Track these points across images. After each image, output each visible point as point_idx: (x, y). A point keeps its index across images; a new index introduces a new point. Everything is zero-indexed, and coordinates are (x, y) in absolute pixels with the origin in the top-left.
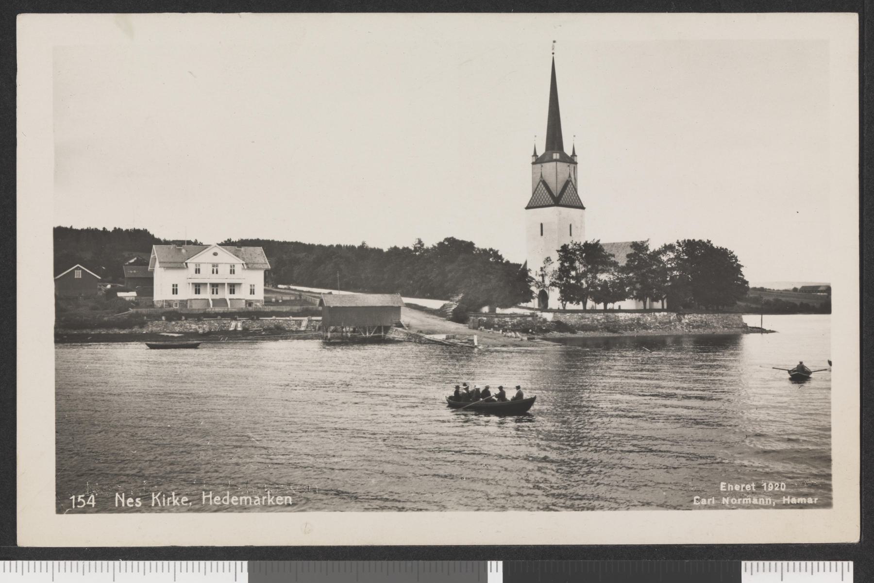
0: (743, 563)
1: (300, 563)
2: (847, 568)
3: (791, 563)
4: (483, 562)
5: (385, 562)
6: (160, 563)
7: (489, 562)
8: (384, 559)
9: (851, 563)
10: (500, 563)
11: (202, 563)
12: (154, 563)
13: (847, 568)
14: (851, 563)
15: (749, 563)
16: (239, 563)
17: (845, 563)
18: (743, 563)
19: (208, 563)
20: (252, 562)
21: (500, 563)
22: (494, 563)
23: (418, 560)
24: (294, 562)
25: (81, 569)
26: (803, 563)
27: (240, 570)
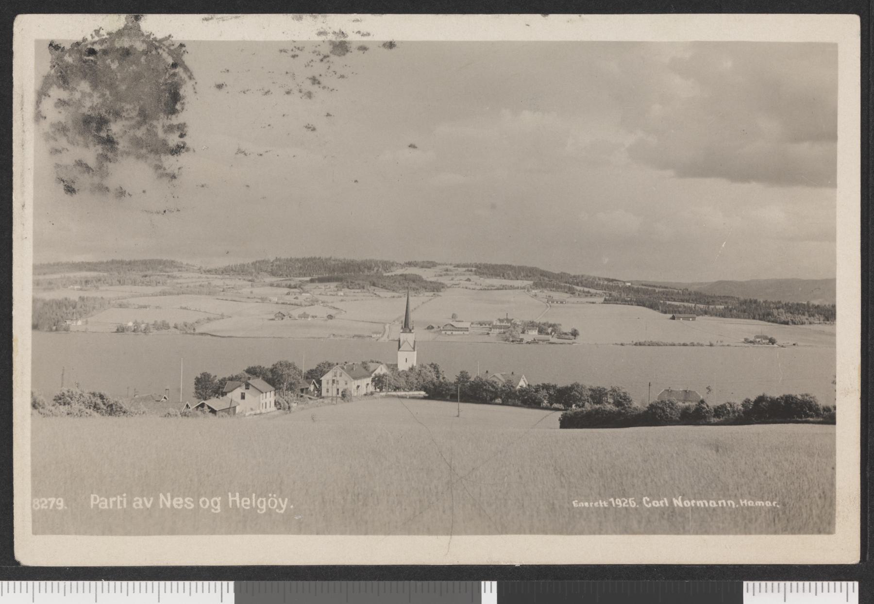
0: (745, 583)
1: (288, 583)
2: (852, 588)
3: (794, 583)
4: (475, 583)
5: (375, 583)
6: (143, 583)
7: (483, 583)
8: (375, 579)
9: (856, 584)
10: (495, 583)
11: (124, 583)
12: (137, 583)
13: (852, 588)
14: (856, 584)
15: (751, 583)
16: (225, 583)
17: (850, 583)
18: (745, 583)
19: (193, 583)
20: (239, 582)
21: (495, 583)
22: (488, 583)
23: (410, 580)
24: (281, 583)
25: (80, 589)
26: (807, 583)
27: (227, 590)
